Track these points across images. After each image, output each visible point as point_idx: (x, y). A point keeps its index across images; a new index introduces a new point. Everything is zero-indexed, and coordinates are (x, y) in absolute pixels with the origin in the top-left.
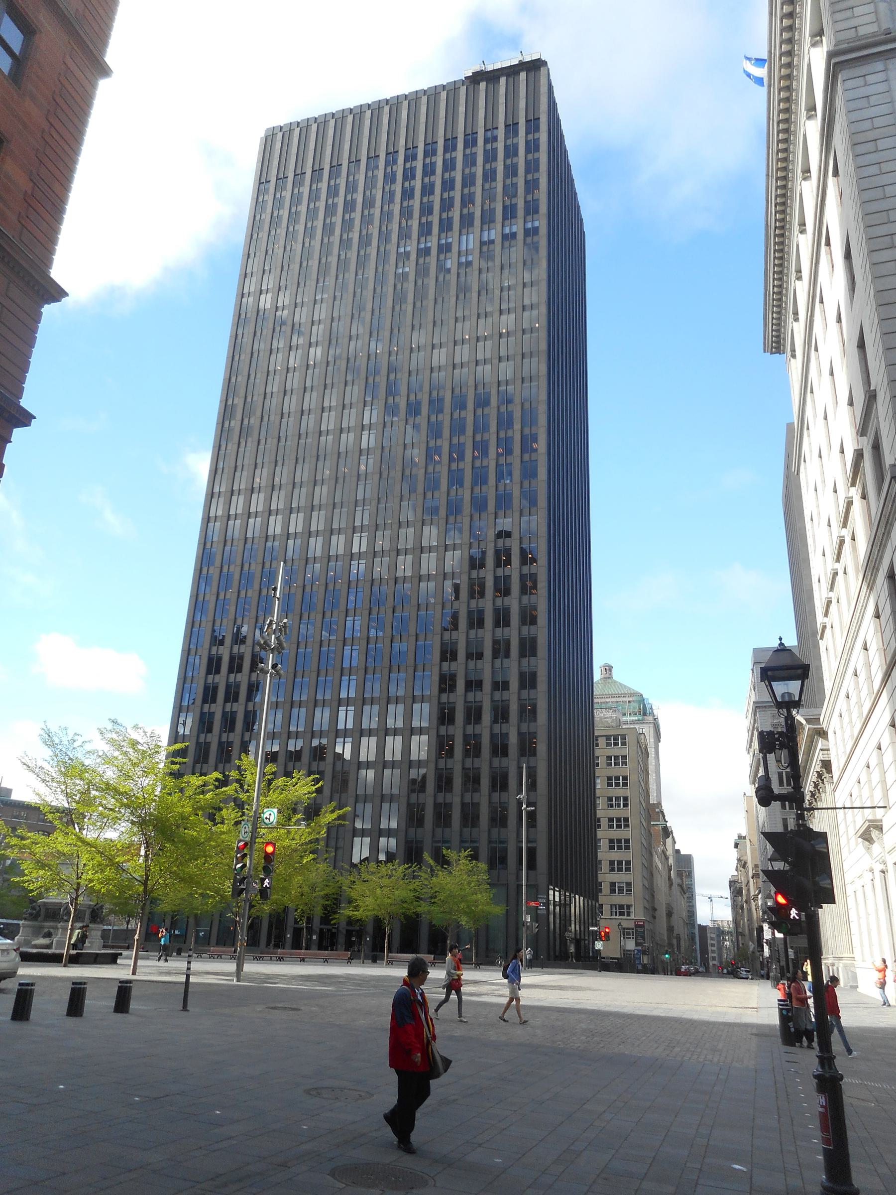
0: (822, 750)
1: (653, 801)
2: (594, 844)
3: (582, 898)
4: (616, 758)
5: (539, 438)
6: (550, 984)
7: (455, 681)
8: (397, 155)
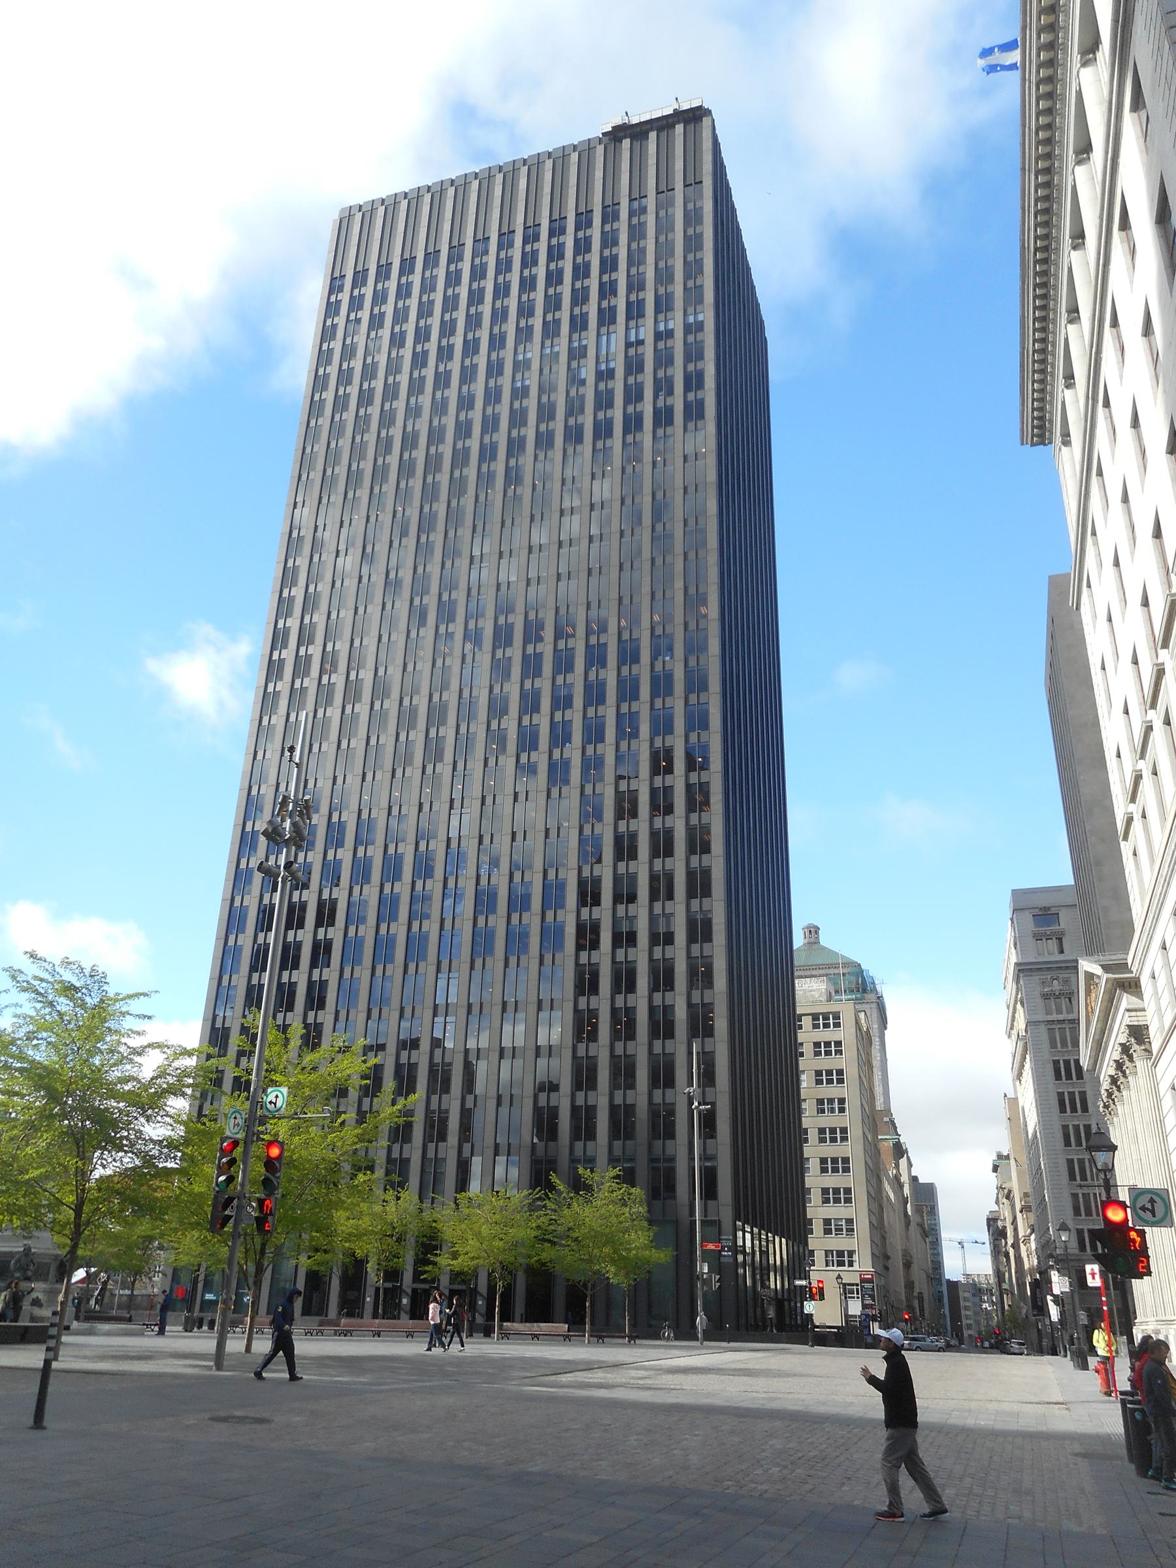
0: (1128, 1010)
1: (879, 1105)
2: (800, 1165)
3: (783, 1240)
4: (828, 1044)
5: (709, 599)
6: (733, 1366)
7: (598, 935)
8: (514, 237)
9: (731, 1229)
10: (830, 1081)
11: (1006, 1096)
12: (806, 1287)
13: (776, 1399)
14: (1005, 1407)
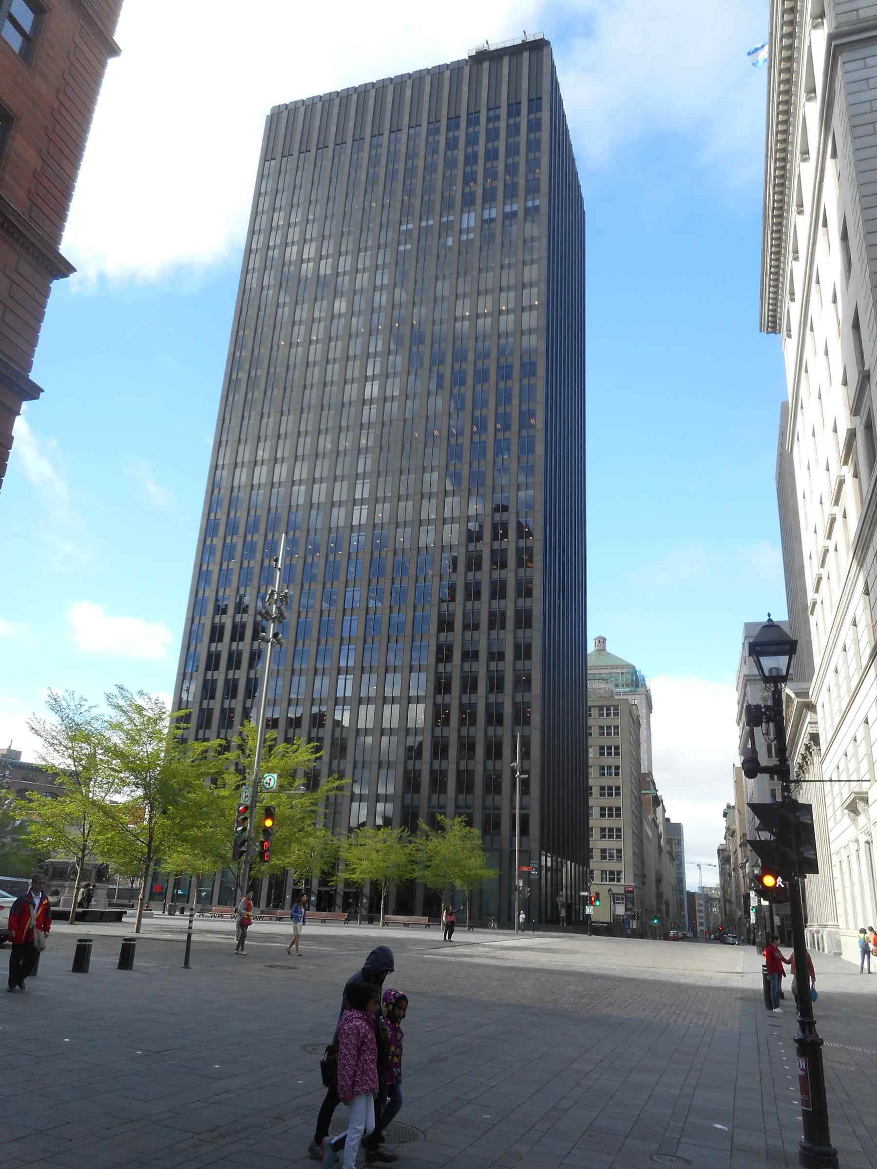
4: (609, 728)
6: (541, 946)
9: (538, 855)
10: (609, 754)
11: (734, 765)
12: (587, 896)
13: (570, 966)
14: (705, 974)
